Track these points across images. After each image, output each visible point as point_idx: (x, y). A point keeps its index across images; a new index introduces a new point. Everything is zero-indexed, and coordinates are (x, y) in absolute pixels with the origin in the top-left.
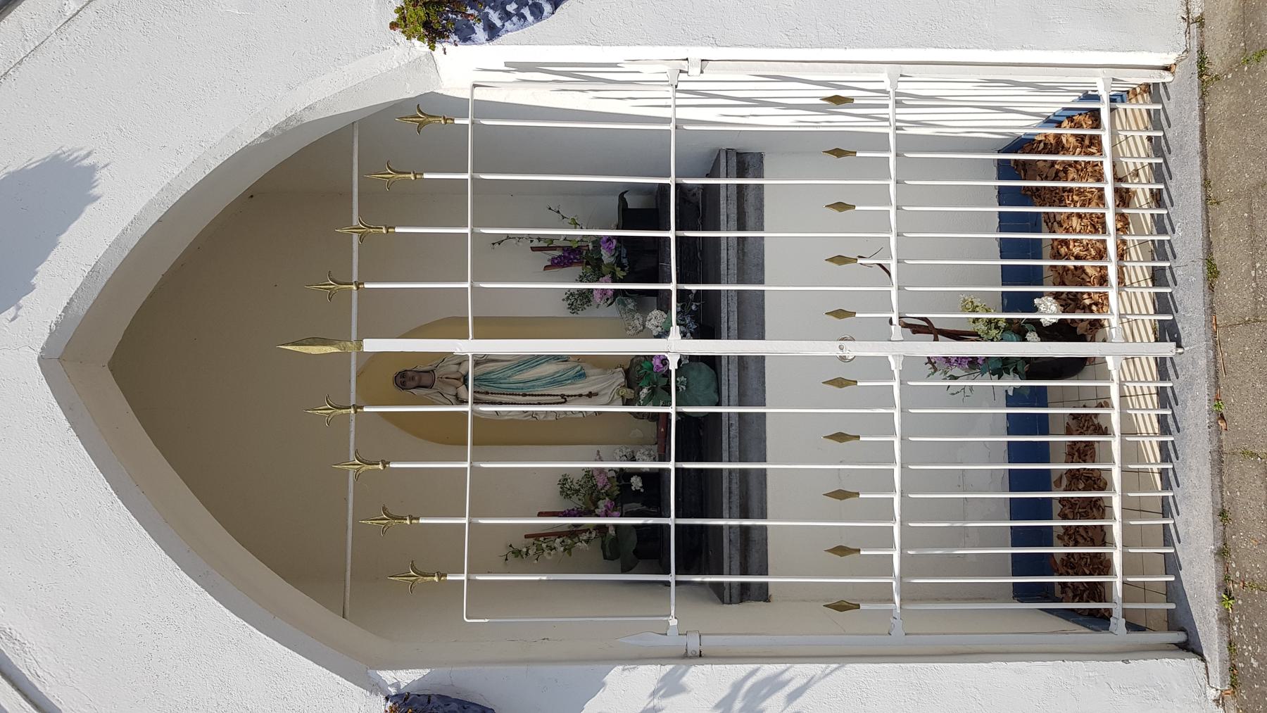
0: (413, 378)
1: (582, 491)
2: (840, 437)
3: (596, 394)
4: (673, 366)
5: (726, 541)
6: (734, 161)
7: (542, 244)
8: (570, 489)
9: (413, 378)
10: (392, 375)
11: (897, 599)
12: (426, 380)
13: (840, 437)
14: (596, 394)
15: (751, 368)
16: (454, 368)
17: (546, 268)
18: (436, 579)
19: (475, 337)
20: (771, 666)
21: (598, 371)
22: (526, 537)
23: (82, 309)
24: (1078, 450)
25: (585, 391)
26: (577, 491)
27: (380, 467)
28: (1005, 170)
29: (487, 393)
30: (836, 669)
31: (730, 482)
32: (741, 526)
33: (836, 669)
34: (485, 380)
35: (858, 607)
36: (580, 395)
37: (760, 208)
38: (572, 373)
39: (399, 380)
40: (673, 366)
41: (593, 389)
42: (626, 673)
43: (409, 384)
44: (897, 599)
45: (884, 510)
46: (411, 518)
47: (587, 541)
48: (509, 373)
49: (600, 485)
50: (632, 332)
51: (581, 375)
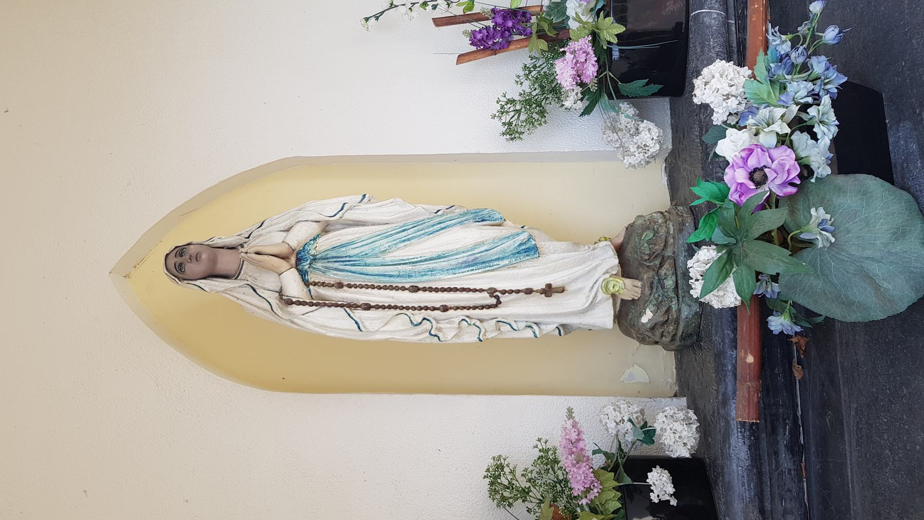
0: (197, 257)
1: (535, 493)
3: (562, 290)
8: (510, 487)
9: (197, 257)
12: (226, 262)
14: (562, 290)
16: (279, 237)
17: (462, 58)
21: (563, 245)
23: (719, 492)
25: (539, 284)
26: (524, 494)
29: (340, 285)
34: (337, 259)
36: (529, 291)
38: (511, 245)
39: (172, 260)
41: (556, 280)
43: (192, 268)
48: (384, 244)
49: (577, 488)
51: (530, 250)
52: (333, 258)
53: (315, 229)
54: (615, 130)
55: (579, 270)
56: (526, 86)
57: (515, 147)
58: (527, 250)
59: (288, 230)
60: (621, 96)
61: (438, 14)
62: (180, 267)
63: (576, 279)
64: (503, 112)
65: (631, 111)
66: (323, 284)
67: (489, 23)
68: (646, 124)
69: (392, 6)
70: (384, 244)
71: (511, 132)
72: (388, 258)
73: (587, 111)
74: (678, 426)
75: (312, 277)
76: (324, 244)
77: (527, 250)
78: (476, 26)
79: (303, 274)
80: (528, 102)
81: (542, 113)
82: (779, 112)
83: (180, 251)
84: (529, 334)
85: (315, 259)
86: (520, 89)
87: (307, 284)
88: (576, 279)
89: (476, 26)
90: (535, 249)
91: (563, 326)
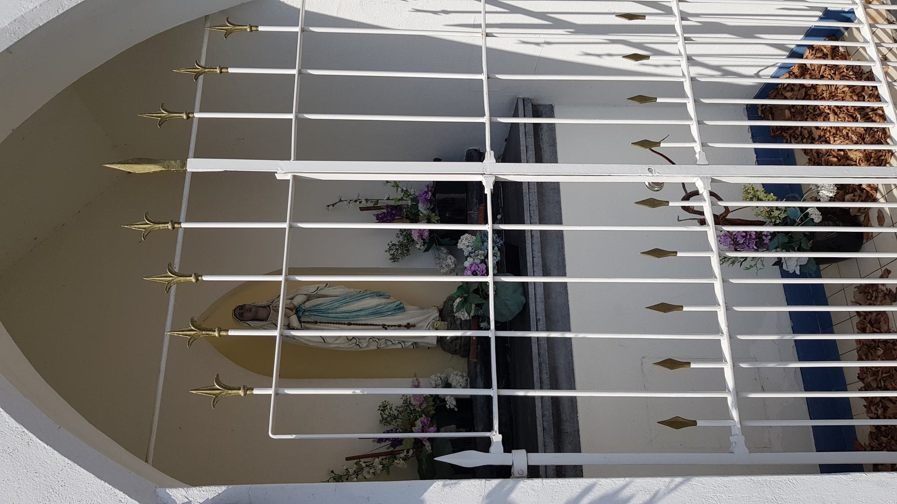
0: (250, 310)
2: (657, 253)
4: (488, 191)
5: (539, 429)
6: (529, 107)
7: (370, 204)
9: (250, 310)
10: (231, 312)
11: (735, 414)
13: (657, 253)
15: (548, 197)
18: (241, 392)
19: (298, 158)
20: (608, 480)
22: (348, 459)
24: (870, 322)
25: (404, 323)
26: (395, 418)
27: (193, 279)
28: (752, 112)
30: (681, 483)
31: (541, 372)
32: (553, 398)
33: (681, 483)
34: (315, 311)
35: (694, 423)
36: (400, 326)
37: (553, 144)
38: (393, 306)
40: (490, 155)
41: (411, 321)
42: (447, 489)
43: (248, 315)
44: (735, 414)
45: (710, 323)
46: (220, 330)
47: (404, 459)
48: (337, 304)
50: (446, 269)
51: (400, 309)
52: (315, 310)
53: (303, 298)
54: (439, 259)
55: (421, 318)
56: (401, 239)
57: (395, 265)
58: (399, 309)
59: (292, 299)
60: (441, 244)
61: (361, 205)
62: (241, 315)
63: (421, 322)
64: (390, 249)
65: (445, 251)
66: (308, 322)
67: (385, 211)
68: (450, 256)
69: (341, 201)
70: (337, 304)
71: (394, 258)
72: (338, 310)
73: (426, 250)
74: (458, 378)
75: (303, 319)
76: (308, 305)
77: (399, 309)
78: (379, 212)
79: (299, 318)
80: (401, 245)
81: (408, 250)
82: (480, 252)
83: (241, 307)
84: (399, 346)
85: (305, 311)
86: (398, 239)
87: (300, 322)
88: (421, 322)
89: (379, 212)
90: (403, 308)
91: (415, 343)
